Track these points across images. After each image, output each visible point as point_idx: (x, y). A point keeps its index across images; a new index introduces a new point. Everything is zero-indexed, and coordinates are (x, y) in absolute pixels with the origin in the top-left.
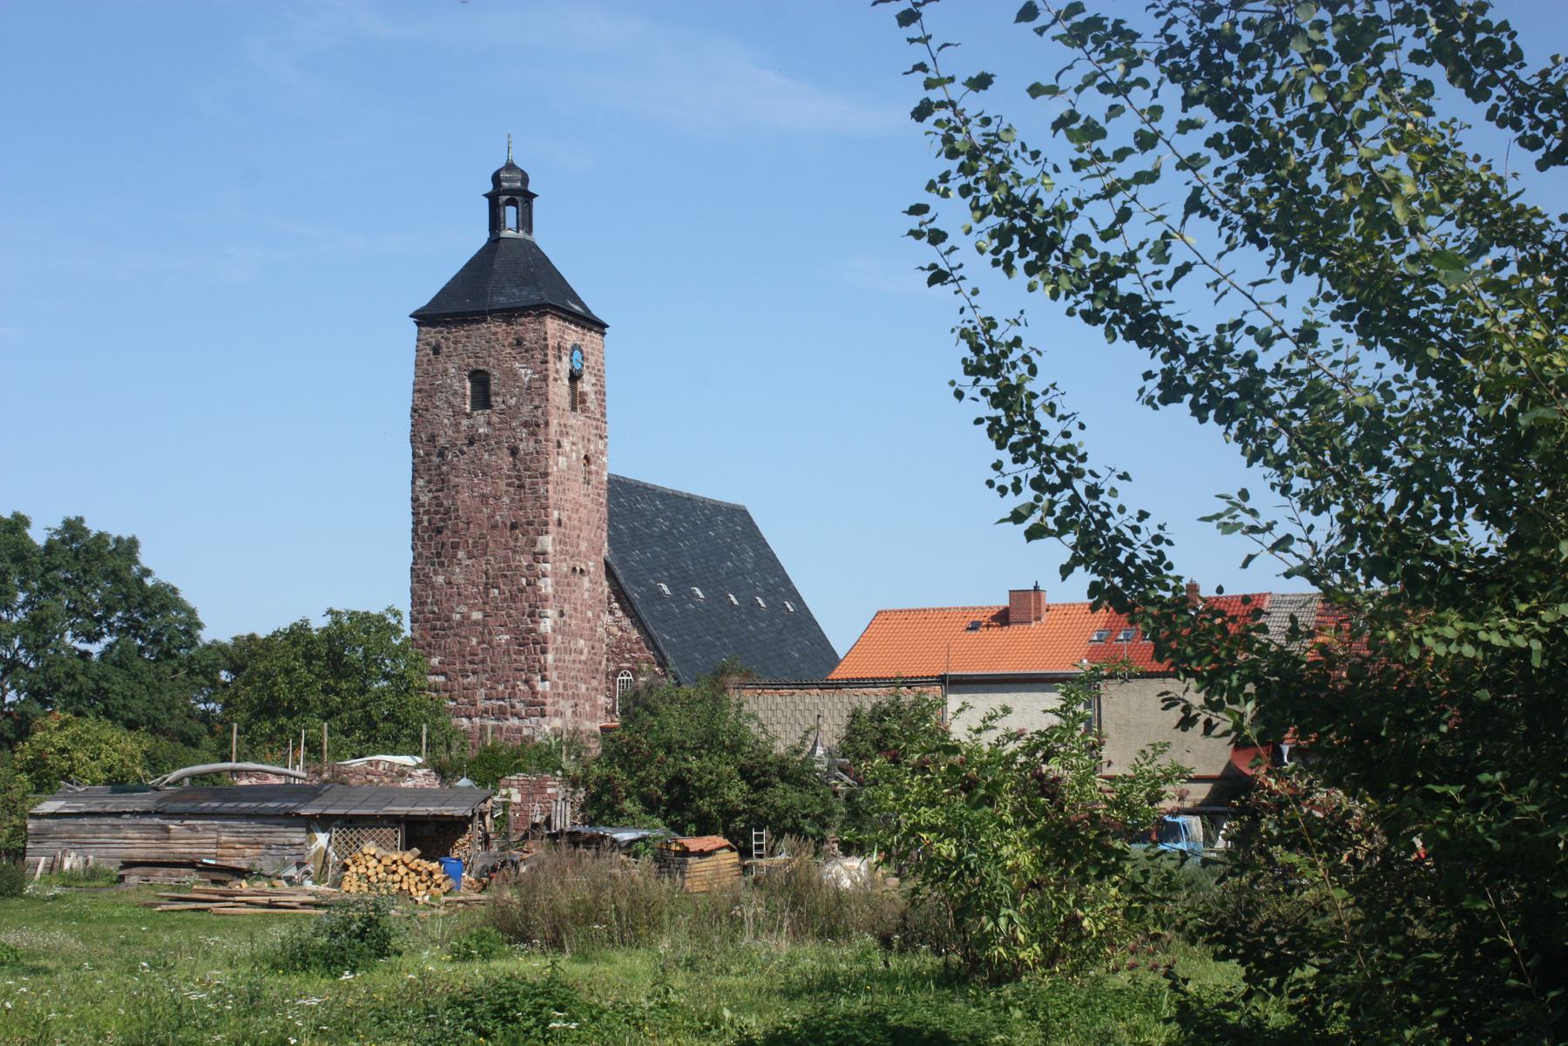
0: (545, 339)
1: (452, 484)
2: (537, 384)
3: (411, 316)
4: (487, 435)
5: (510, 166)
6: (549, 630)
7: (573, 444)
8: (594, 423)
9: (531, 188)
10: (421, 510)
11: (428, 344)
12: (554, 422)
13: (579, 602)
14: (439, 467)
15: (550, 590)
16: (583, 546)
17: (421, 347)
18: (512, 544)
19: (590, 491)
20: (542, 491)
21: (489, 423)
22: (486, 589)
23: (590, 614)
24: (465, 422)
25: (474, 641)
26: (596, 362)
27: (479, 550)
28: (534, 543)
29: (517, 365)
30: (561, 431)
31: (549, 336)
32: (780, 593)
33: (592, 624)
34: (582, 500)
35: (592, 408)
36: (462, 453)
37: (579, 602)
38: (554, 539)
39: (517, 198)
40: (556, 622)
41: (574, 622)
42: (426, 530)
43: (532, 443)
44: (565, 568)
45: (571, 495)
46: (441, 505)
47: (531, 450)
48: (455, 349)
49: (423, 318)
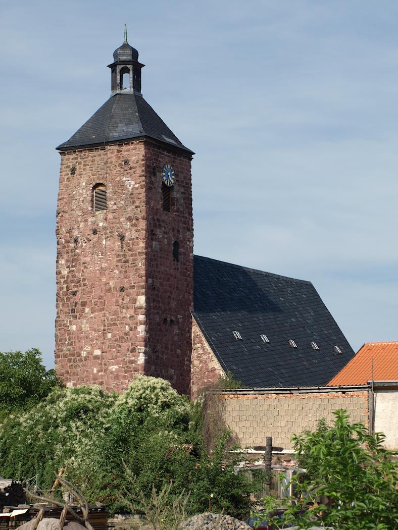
1: (82, 262)
5: (126, 46)
7: (165, 233)
10: (62, 280)
11: (68, 167)
14: (73, 251)
16: (173, 304)
18: (121, 301)
19: (179, 266)
25: (95, 371)
27: (100, 306)
29: (124, 179)
30: (155, 224)
32: (333, 340)
39: (128, 66)
41: (165, 356)
48: (84, 169)
49: (63, 149)
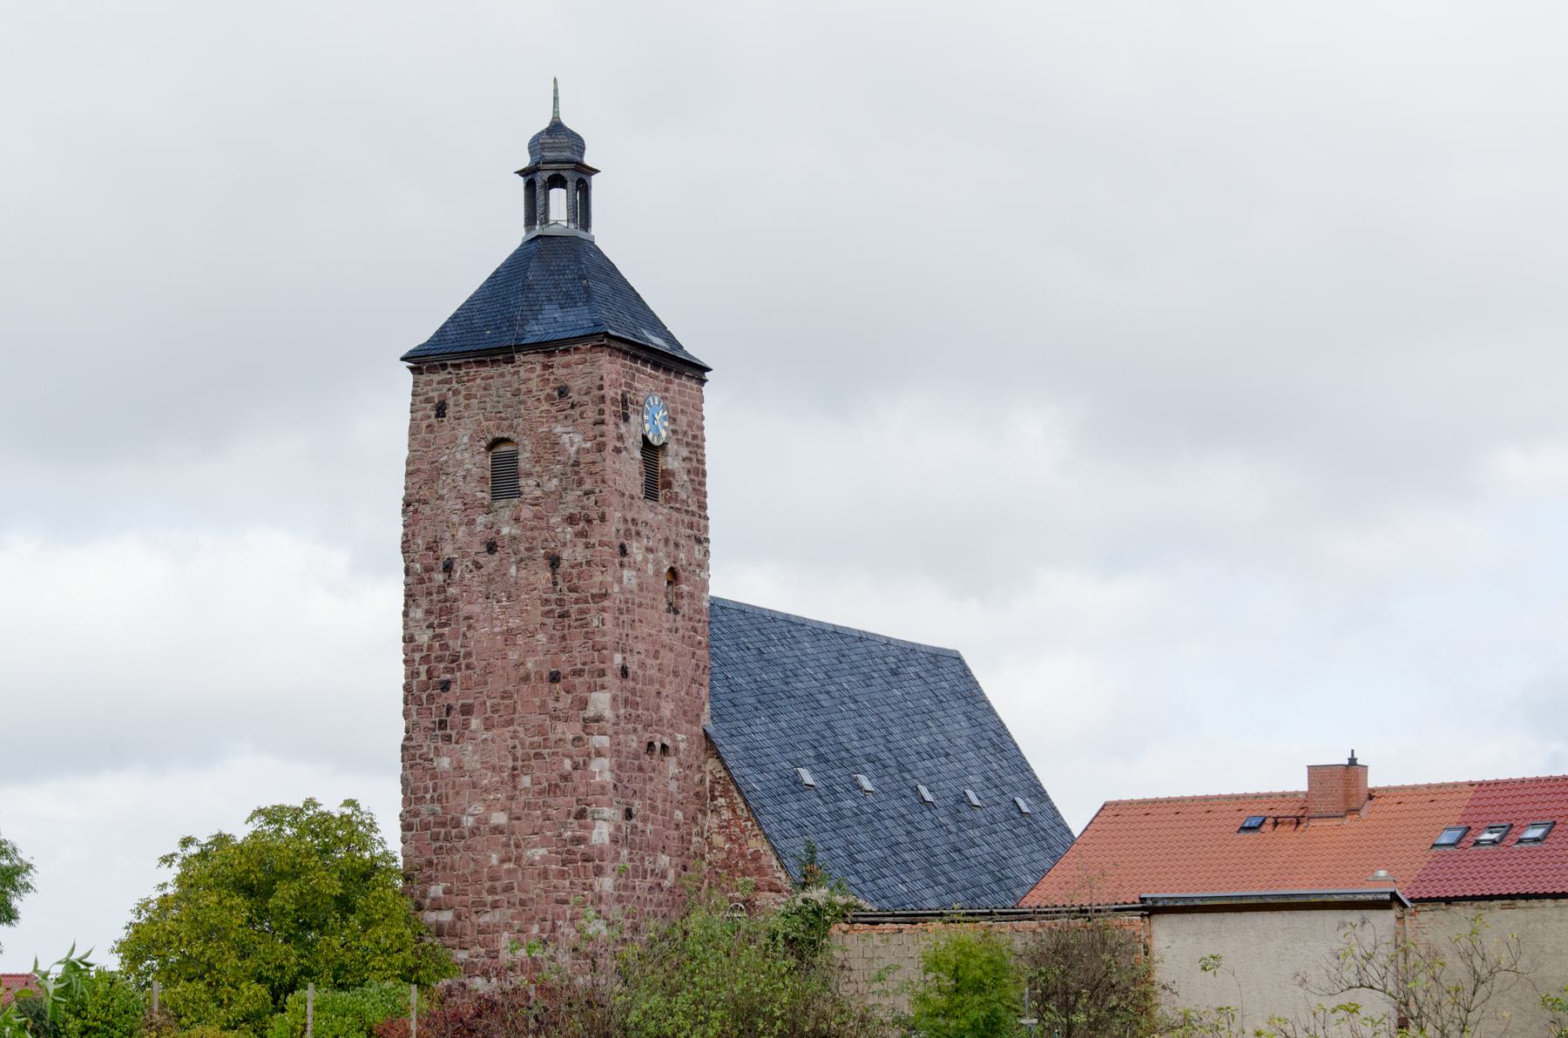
0: (601, 388)
1: (462, 614)
2: (590, 457)
3: (403, 359)
4: (514, 538)
6: (607, 841)
7: (650, 550)
8: (687, 518)
9: (588, 160)
10: (417, 656)
12: (615, 516)
13: (660, 796)
14: (442, 589)
15: (608, 777)
16: (667, 710)
17: (419, 405)
20: (596, 623)
21: (517, 520)
22: (514, 777)
23: (679, 815)
24: (481, 519)
26: (690, 425)
28: (584, 704)
29: (558, 429)
30: (628, 531)
31: (606, 383)
33: (683, 830)
34: (665, 637)
35: (683, 496)
36: (478, 566)
37: (660, 796)
38: (614, 699)
40: (618, 828)
41: (650, 827)
42: (424, 687)
43: (580, 549)
44: (634, 743)
45: (643, 630)
46: (444, 647)
47: (579, 559)
49: (420, 361)
